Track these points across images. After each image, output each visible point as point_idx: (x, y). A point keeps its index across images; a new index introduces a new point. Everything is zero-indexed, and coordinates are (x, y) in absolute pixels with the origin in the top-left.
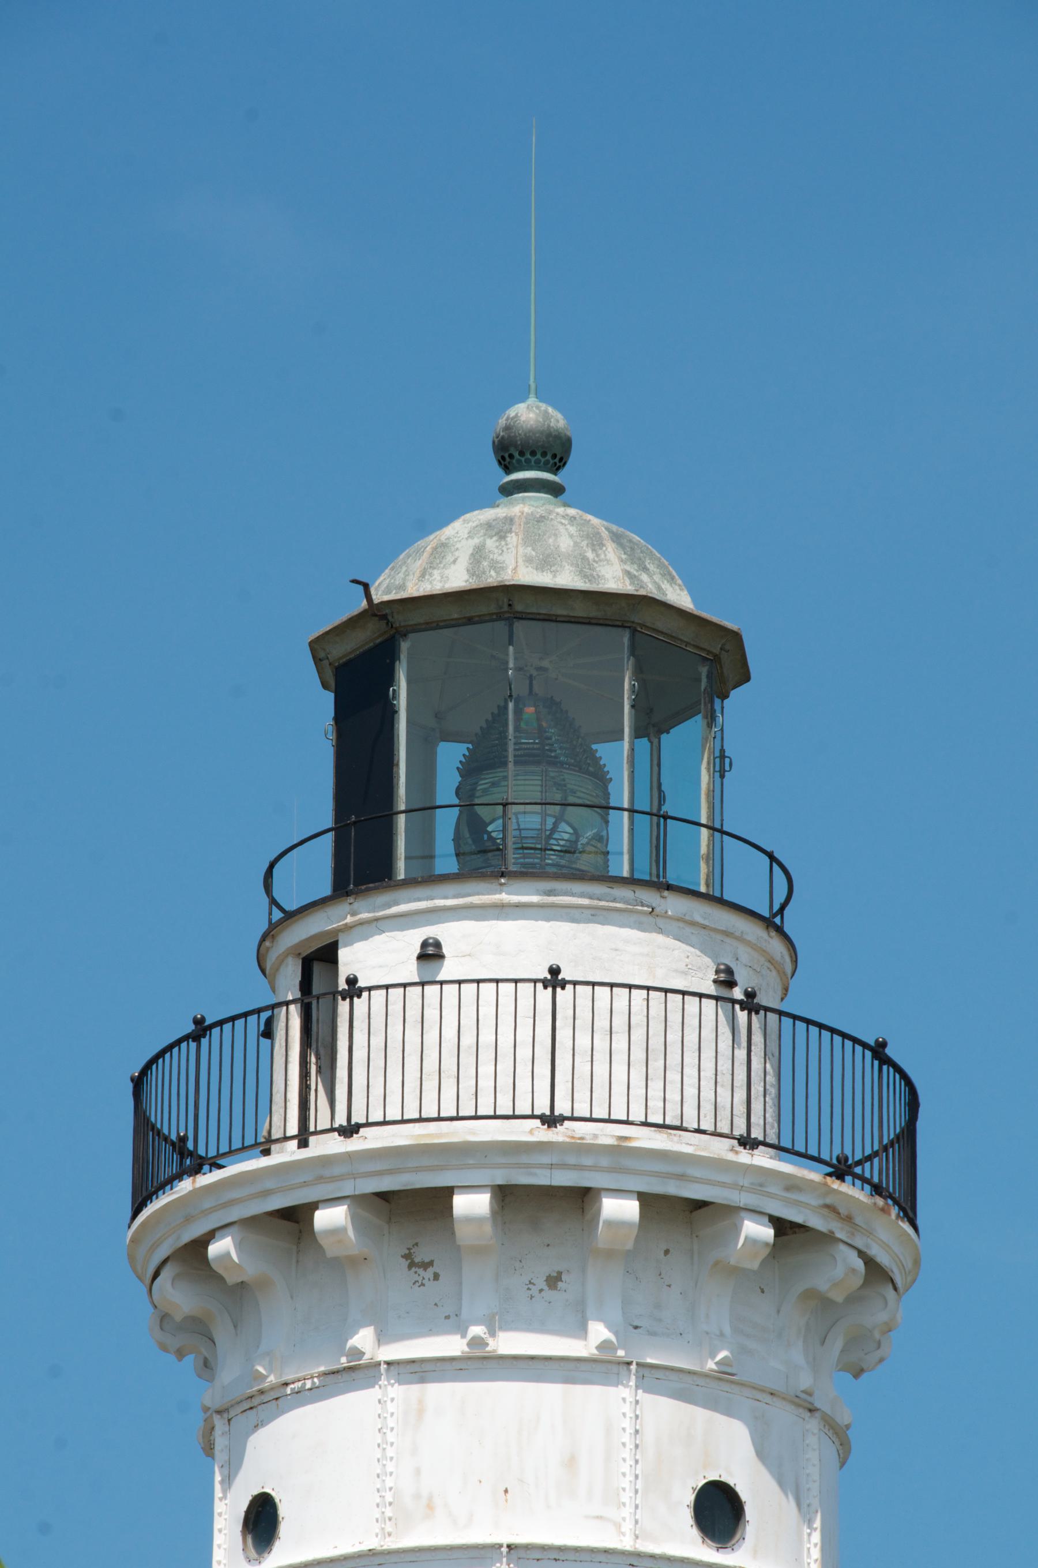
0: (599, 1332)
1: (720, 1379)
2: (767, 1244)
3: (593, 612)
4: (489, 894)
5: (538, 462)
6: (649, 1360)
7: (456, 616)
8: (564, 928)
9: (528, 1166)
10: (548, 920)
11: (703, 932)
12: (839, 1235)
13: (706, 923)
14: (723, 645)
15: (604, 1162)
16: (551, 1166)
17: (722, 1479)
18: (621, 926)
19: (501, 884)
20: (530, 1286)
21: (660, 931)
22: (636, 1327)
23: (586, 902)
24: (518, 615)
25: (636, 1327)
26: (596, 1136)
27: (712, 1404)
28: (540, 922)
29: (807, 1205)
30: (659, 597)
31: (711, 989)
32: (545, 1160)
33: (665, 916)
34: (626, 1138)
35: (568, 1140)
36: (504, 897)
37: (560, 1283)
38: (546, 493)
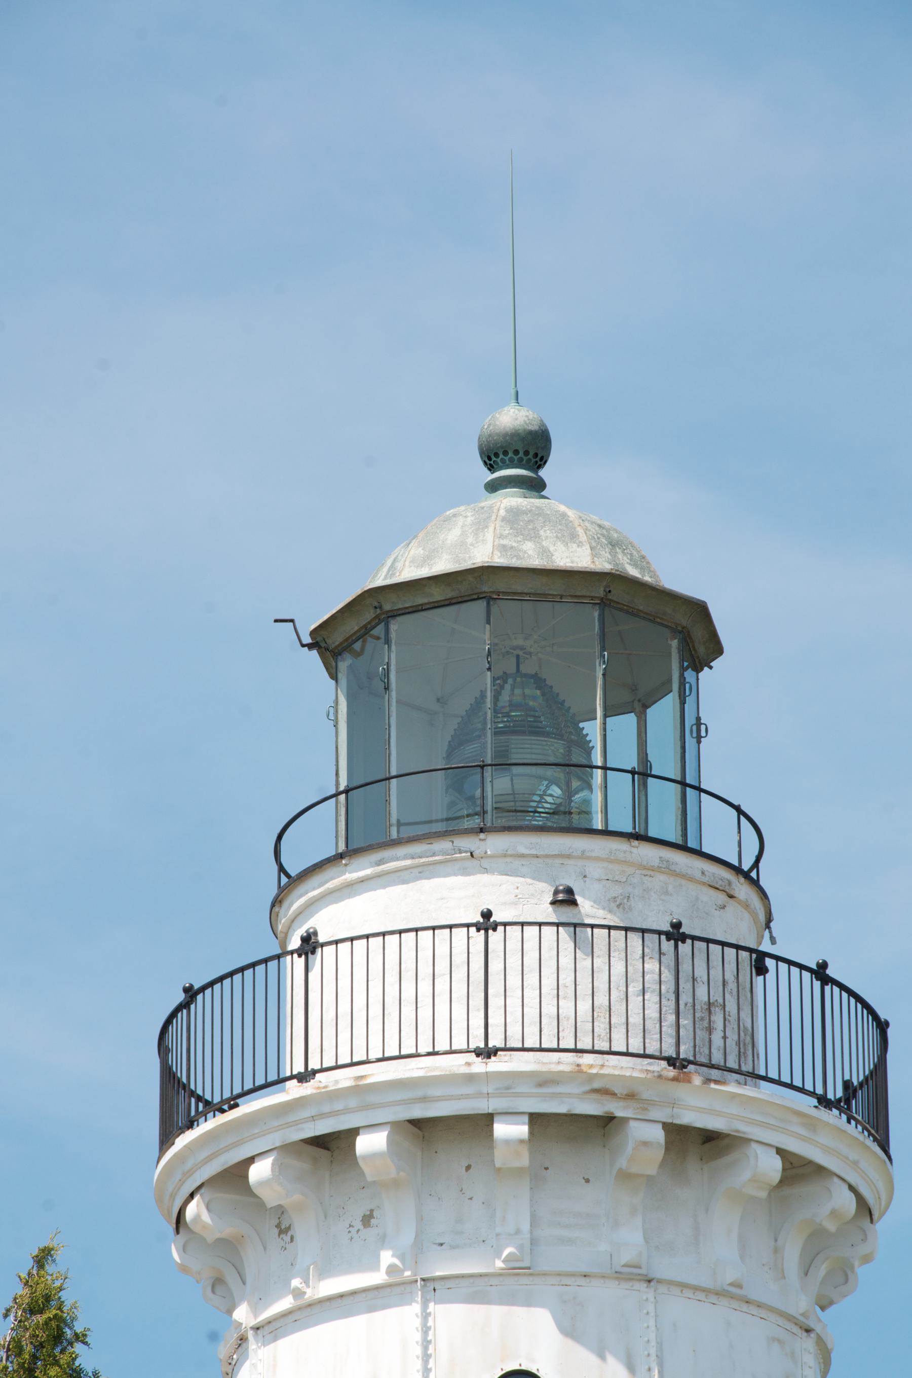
0: (387, 1258)
1: (510, 1275)
2: (522, 1141)
3: (449, 594)
4: (339, 877)
5: (511, 460)
6: (438, 1274)
7: (356, 628)
8: (397, 891)
9: (296, 1123)
10: (384, 887)
11: (536, 861)
12: (619, 1113)
13: (534, 852)
14: (606, 587)
15: (353, 1103)
16: (313, 1118)
17: (523, 1368)
18: (445, 876)
19: (346, 865)
20: (351, 1229)
21: (486, 871)
22: (441, 1245)
23: (408, 862)
24: (390, 614)
25: (441, 1245)
26: (337, 1082)
27: (510, 1300)
28: (378, 891)
29: (569, 1095)
30: (515, 563)
31: (547, 913)
32: (306, 1113)
33: (485, 856)
34: (362, 1077)
35: (315, 1091)
36: (350, 876)
37: (372, 1220)
38: (514, 487)
